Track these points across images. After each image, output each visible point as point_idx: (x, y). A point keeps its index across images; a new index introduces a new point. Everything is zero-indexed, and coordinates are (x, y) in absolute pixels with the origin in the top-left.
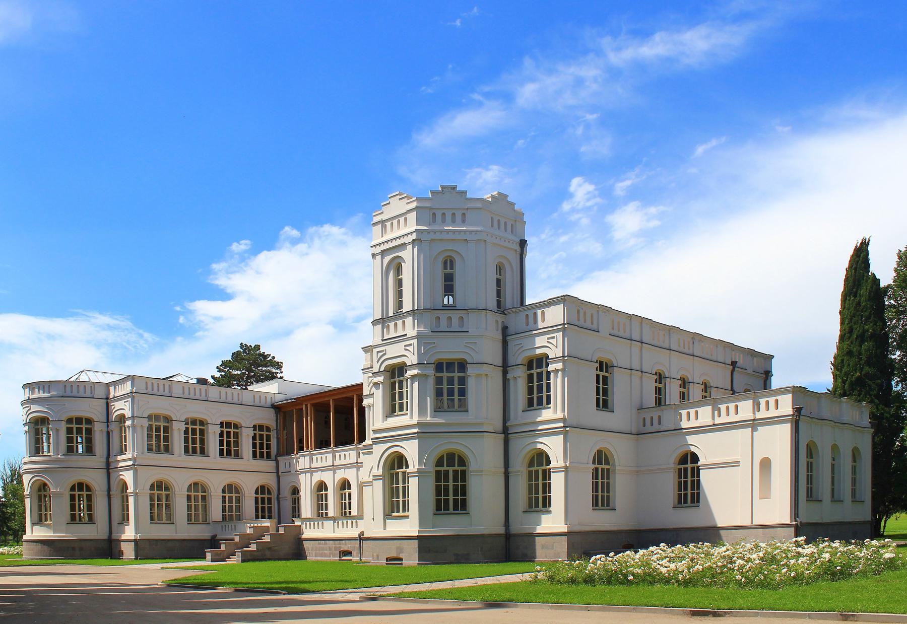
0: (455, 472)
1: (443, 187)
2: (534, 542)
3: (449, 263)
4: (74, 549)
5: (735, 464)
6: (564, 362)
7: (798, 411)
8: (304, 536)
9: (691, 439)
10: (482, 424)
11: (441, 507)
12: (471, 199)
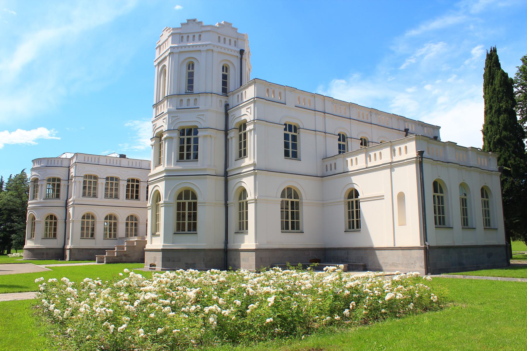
0: (190, 204)
1: (188, 21)
2: (375, 255)
3: (191, 66)
4: (43, 254)
5: (380, 198)
6: (255, 124)
7: (421, 153)
8: (148, 246)
9: (355, 179)
10: (205, 170)
11: (180, 228)
12: (204, 26)
